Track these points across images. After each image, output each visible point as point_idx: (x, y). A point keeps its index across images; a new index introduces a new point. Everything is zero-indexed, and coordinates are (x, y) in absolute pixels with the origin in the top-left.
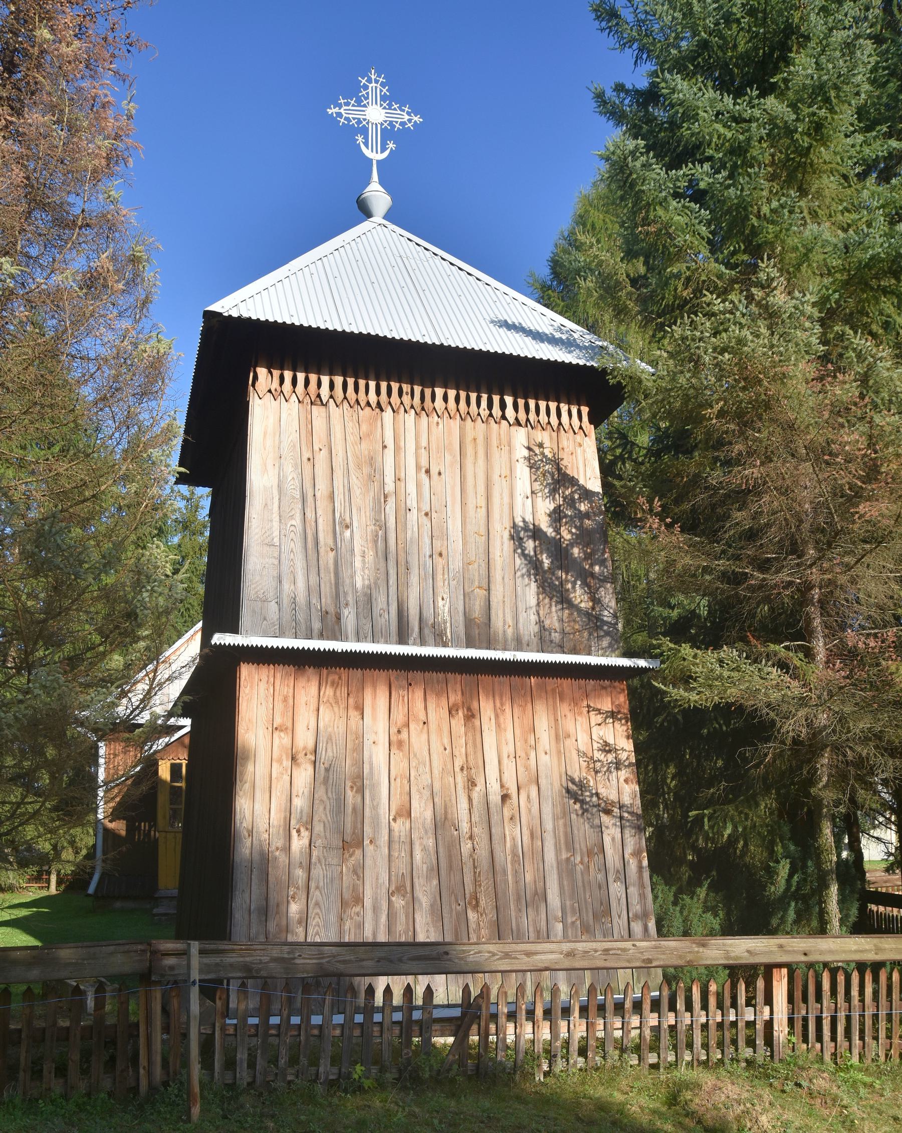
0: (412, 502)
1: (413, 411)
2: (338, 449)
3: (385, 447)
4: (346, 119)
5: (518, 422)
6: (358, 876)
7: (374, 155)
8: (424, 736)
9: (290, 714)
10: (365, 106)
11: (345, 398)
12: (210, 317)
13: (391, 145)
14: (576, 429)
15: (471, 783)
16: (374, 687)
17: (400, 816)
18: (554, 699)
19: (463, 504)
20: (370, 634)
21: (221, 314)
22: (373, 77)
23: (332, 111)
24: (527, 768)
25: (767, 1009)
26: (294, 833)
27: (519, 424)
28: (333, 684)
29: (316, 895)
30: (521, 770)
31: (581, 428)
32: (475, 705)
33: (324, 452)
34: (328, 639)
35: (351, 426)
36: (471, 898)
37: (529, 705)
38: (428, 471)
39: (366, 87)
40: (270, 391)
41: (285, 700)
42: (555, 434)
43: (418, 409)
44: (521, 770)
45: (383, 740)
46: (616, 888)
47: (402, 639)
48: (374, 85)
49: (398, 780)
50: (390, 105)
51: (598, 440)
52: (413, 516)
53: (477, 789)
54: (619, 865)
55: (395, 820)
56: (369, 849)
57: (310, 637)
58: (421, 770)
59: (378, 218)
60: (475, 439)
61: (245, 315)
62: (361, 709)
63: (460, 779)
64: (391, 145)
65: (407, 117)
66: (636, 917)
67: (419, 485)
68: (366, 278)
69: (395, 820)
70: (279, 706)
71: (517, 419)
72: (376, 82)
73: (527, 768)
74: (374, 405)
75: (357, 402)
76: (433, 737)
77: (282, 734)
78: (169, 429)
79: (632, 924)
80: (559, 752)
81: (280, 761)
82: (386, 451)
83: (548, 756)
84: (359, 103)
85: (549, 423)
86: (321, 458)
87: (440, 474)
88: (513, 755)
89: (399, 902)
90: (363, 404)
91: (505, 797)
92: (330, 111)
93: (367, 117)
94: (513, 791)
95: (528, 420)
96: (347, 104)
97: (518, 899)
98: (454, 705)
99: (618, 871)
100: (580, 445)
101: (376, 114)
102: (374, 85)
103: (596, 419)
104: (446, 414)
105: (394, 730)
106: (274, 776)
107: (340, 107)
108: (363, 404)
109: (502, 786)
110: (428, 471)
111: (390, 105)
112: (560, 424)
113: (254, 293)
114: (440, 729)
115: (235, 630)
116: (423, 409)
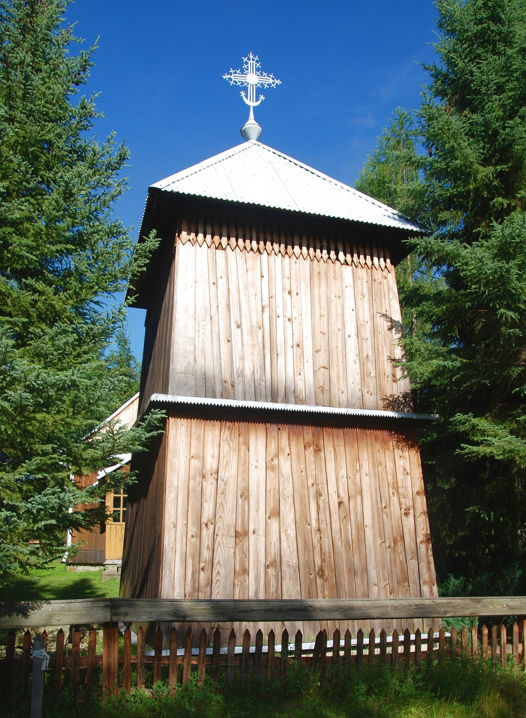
0: (280, 312)
1: (280, 254)
2: (233, 277)
3: (262, 276)
4: (234, 82)
5: (346, 263)
6: (245, 555)
7: (252, 103)
8: (289, 463)
9: (202, 448)
10: (246, 74)
11: (237, 245)
12: (155, 193)
13: (262, 98)
14: (383, 267)
15: (319, 494)
16: (256, 433)
17: (273, 515)
18: (371, 439)
19: (313, 314)
20: (253, 396)
21: (160, 189)
22: (251, 57)
23: (226, 77)
24: (355, 484)
25: (520, 647)
26: (204, 526)
27: (348, 265)
28: (229, 428)
29: (216, 568)
30: (351, 485)
31: (386, 267)
32: (321, 442)
33: (224, 278)
34: (226, 398)
35: (241, 262)
36: (319, 571)
37: (356, 443)
38: (290, 293)
39: (247, 63)
40: (189, 240)
41: (198, 438)
42: (369, 271)
43: (283, 253)
44: (351, 485)
45: (262, 464)
46: (413, 563)
47: (274, 400)
48: (252, 62)
49: (272, 492)
50: (261, 74)
51: (397, 273)
52: (280, 321)
53: (323, 498)
54: (414, 548)
55: (269, 518)
56: (252, 537)
57: (214, 397)
58: (286, 484)
59: (253, 141)
60: (319, 273)
61: (175, 190)
62: (247, 445)
63: (312, 492)
64: (262, 98)
65: (272, 81)
66: (425, 583)
67: (284, 301)
68: (250, 172)
69: (269, 518)
70: (194, 442)
71: (345, 261)
72: (253, 60)
73: (355, 484)
74: (255, 250)
75: (245, 247)
76: (294, 464)
77: (196, 461)
78: (27, 574)
79: (422, 587)
80: (375, 474)
81: (195, 478)
82: (263, 279)
83: (368, 477)
84: (242, 72)
85: (366, 263)
86: (222, 283)
87: (297, 294)
88: (345, 476)
89: (271, 571)
90: (248, 249)
91: (340, 503)
92: (224, 77)
93: (247, 81)
94: (345, 500)
95: (353, 261)
96: (235, 73)
97: (349, 571)
98: (307, 443)
99: (413, 552)
100: (386, 278)
101: (252, 79)
102: (251, 61)
103: (394, 263)
104: (301, 257)
105: (269, 458)
106: (191, 488)
107: (231, 74)
108: (248, 249)
109: (338, 496)
110: (290, 293)
111: (261, 74)
112: (373, 264)
113: (180, 178)
114: (298, 458)
115: (165, 391)
116: (286, 253)
